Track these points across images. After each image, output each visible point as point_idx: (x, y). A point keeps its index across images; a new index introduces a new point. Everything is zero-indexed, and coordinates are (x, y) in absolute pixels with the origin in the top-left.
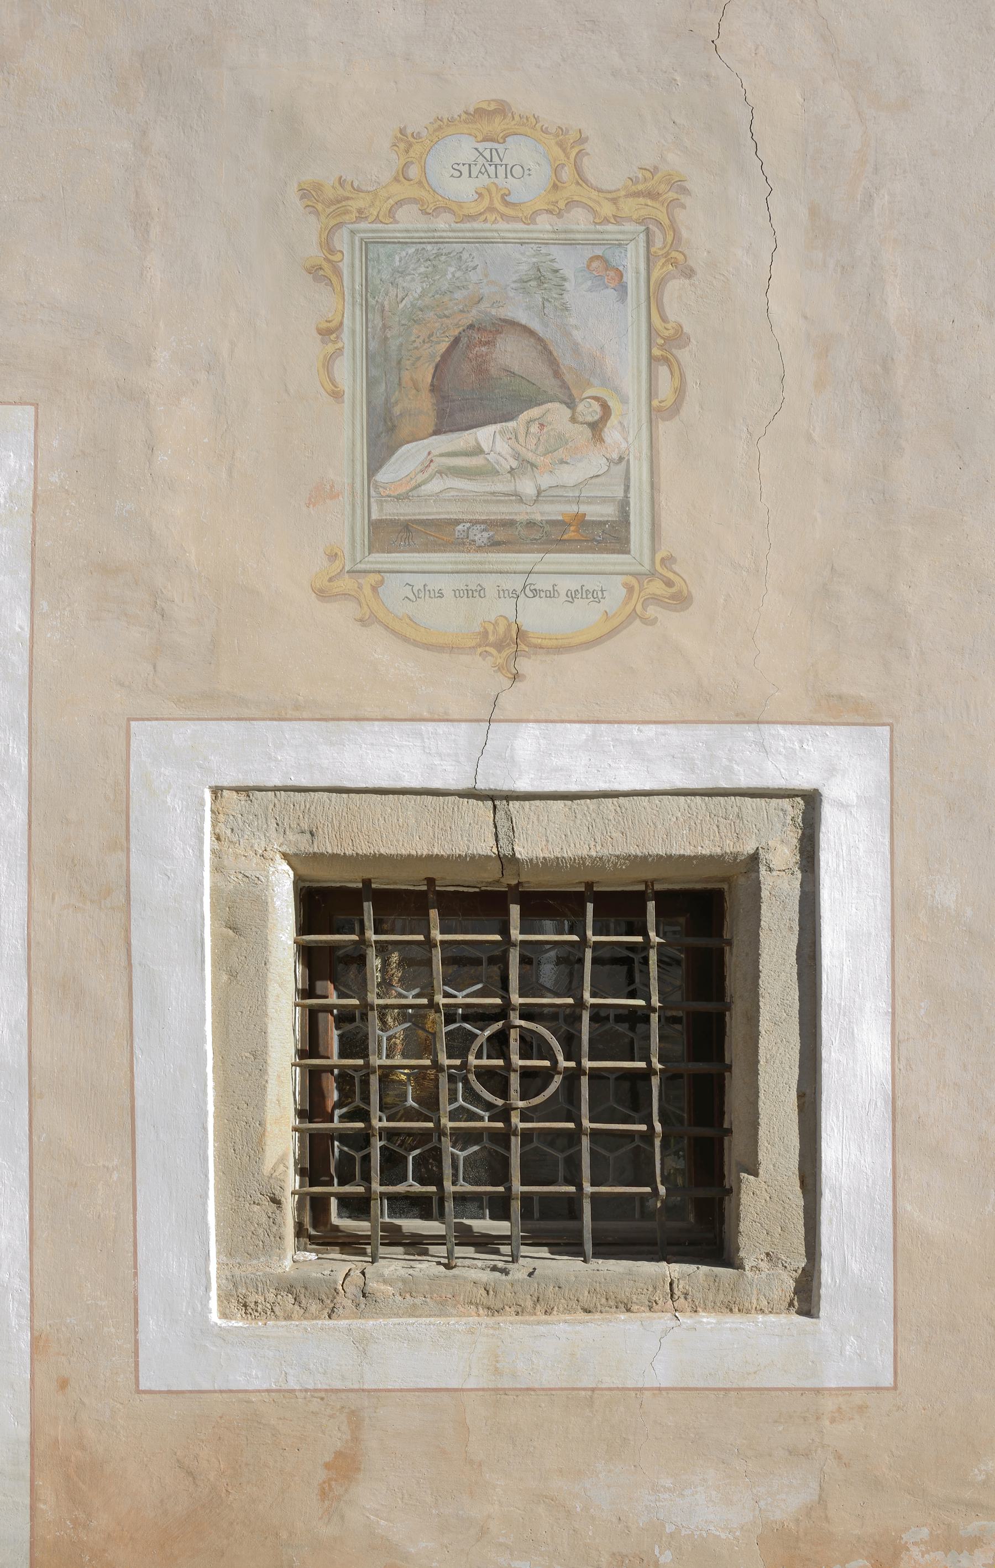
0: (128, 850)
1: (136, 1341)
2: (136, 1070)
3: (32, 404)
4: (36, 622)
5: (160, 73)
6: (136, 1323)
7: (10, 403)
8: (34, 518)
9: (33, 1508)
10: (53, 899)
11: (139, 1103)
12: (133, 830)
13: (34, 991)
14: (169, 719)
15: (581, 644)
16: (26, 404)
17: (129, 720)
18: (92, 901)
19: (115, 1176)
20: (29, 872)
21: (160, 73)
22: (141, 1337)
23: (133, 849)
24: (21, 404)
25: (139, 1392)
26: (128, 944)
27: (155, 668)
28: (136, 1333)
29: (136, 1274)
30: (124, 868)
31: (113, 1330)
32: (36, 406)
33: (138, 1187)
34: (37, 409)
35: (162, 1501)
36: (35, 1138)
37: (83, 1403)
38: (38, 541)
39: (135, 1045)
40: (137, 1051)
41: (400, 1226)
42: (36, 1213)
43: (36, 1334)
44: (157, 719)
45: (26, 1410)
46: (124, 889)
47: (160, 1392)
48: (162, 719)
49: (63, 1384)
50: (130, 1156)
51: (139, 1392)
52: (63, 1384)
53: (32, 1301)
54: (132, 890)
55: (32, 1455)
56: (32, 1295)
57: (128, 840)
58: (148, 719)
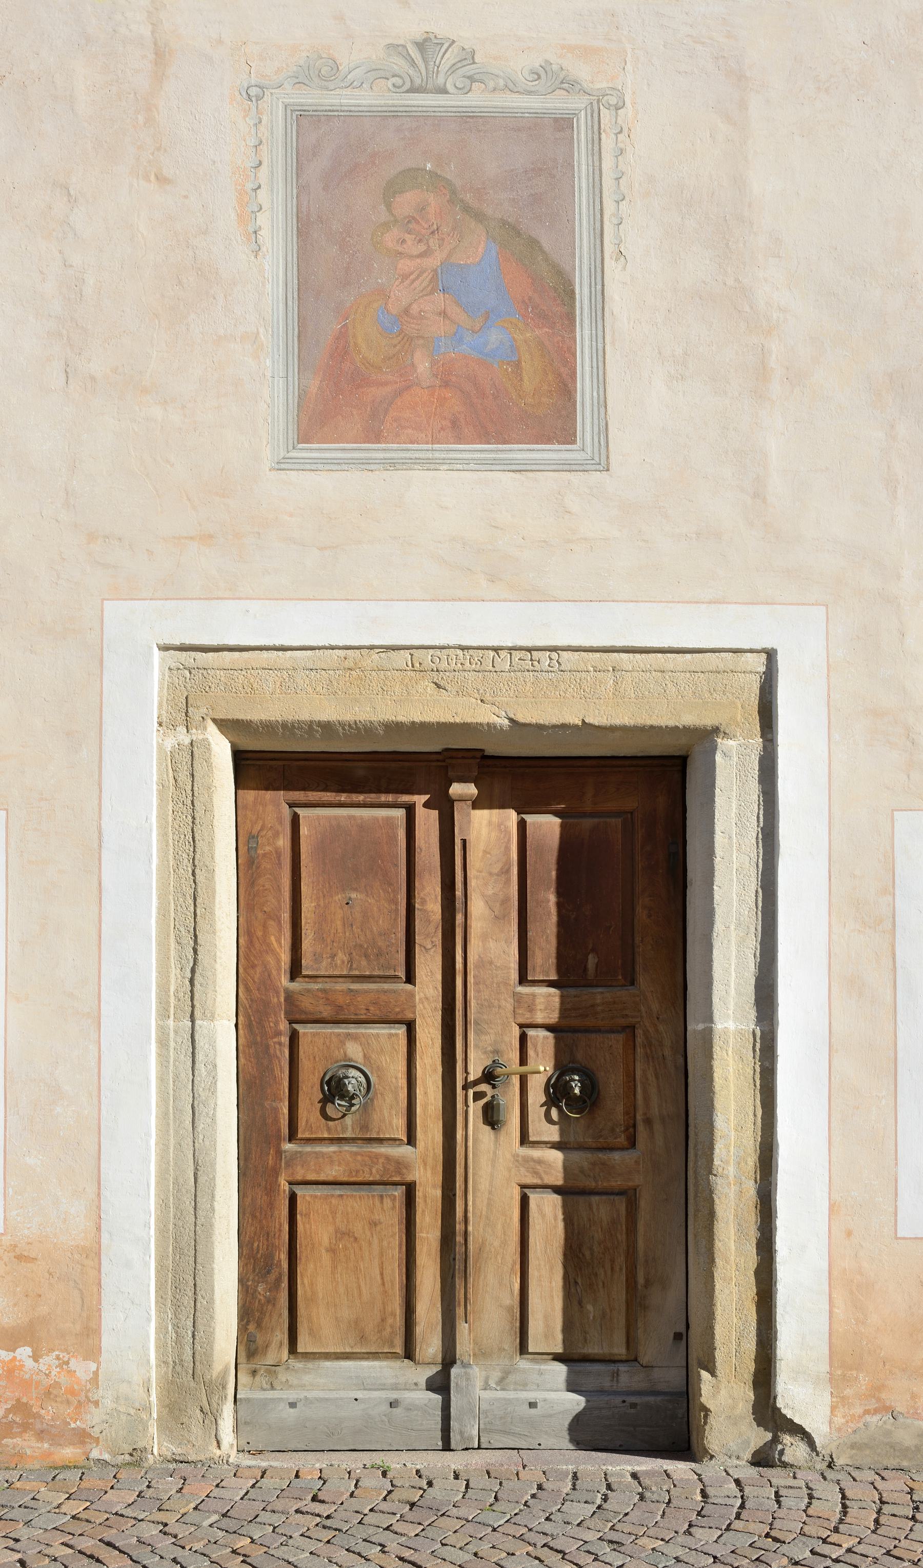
0: (894, 894)
1: (896, 1206)
2: (899, 1034)
3: (824, 605)
4: (831, 747)
5: (903, 387)
6: (896, 1194)
7: (809, 605)
8: (828, 680)
9: (831, 1312)
10: (845, 926)
11: (900, 1056)
12: (897, 882)
13: (832, 983)
14: (919, 810)
15: (371, 804)
16: (821, 605)
17: (893, 810)
18: (870, 927)
19: (884, 1102)
20: (830, 908)
21: (903, 387)
22: (899, 1203)
23: (897, 893)
24: (816, 605)
25: (897, 1238)
26: (894, 955)
27: (908, 777)
28: (896, 1201)
29: (896, 1164)
30: (892, 906)
31: (881, 1199)
32: (827, 606)
33: (898, 1109)
34: (827, 608)
35: (910, 1307)
36: (833, 1079)
37: (862, 1246)
38: (832, 696)
39: (898, 1019)
40: (899, 1022)
41: (568, 1391)
42: (832, 1125)
43: (832, 1202)
44: (911, 810)
45: (826, 1250)
46: (891, 919)
47: (910, 1238)
48: (915, 810)
49: (849, 1234)
50: (893, 1089)
51: (897, 1238)
52: (849, 1234)
53: (830, 1181)
54: (897, 919)
55: (830, 1278)
56: (830, 1178)
57: (894, 887)
58: (905, 810)
